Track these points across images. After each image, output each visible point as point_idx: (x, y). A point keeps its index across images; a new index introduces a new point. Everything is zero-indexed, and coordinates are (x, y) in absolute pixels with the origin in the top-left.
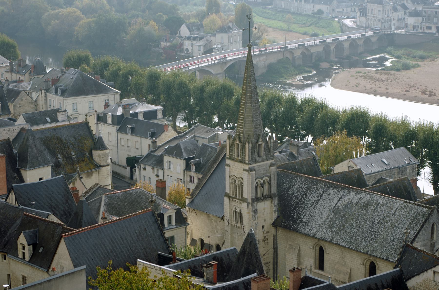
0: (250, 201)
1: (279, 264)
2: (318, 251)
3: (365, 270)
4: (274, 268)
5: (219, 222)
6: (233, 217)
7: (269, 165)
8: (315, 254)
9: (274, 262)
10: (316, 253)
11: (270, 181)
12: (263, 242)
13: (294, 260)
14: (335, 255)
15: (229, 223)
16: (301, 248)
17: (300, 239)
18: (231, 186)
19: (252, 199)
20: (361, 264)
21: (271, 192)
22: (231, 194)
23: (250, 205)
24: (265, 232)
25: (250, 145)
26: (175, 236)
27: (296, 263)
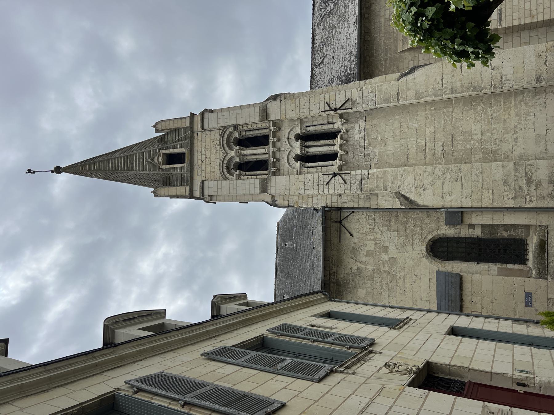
17: (383, 20)
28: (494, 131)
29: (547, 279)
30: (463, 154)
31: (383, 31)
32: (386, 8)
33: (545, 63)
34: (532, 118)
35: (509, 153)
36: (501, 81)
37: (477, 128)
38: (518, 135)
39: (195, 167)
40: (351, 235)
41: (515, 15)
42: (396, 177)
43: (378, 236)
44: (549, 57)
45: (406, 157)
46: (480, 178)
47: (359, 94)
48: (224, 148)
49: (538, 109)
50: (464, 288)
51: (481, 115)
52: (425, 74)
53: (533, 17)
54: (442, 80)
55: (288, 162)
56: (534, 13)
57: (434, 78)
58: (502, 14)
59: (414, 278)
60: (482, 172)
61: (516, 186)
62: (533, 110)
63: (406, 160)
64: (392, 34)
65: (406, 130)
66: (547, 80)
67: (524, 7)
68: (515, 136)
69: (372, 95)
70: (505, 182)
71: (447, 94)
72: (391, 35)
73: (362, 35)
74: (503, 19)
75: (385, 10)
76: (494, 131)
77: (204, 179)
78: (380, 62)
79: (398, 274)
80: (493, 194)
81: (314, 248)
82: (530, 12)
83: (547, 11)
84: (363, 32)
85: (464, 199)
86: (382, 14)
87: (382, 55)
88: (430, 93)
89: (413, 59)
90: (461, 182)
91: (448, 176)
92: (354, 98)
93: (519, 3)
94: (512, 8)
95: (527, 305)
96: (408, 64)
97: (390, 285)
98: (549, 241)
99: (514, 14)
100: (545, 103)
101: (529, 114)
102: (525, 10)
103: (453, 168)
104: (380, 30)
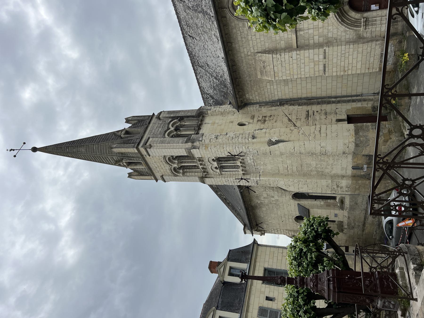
0: (189, 145)
1: (309, 95)
4: (318, 103)
5: (256, 193)
6: (231, 173)
9: (305, 104)
11: (178, 117)
12: (266, 123)
13: (283, 60)
15: (242, 179)
16: (260, 50)
17: (243, 55)
18: (188, 174)
19: (186, 142)
22: (199, 174)
23: (195, 144)
24: (251, 121)
26: (266, 266)
27: (287, 54)
28: (322, 165)
29: (343, 210)
30: (307, 171)
31: (244, 63)
32: (244, 47)
33: (348, 147)
34: (340, 161)
35: (329, 173)
36: (326, 152)
37: (314, 163)
38: (334, 167)
39: (153, 169)
40: (255, 192)
41: (334, 69)
42: (275, 181)
43: (268, 193)
44: (350, 145)
45: (278, 171)
46: (316, 184)
47: (247, 150)
48: (168, 164)
49: (343, 158)
50: (310, 212)
51: (316, 158)
52: (285, 145)
53: (345, 71)
54: (294, 148)
55: (212, 170)
56: (346, 69)
57: (290, 148)
58: (326, 68)
59: (287, 205)
60: (317, 183)
61: (332, 188)
62: (341, 158)
63: (278, 172)
64: (252, 65)
65: (277, 161)
66: (348, 154)
67: (340, 65)
68: (332, 167)
69: (255, 151)
70: (327, 186)
71: (297, 154)
72: (251, 66)
73: (230, 66)
74: (326, 71)
75: (244, 48)
76: (322, 165)
77: (161, 175)
78: (247, 82)
79: (280, 204)
80: (322, 189)
81: (234, 189)
82: (344, 68)
83: (354, 68)
84: (230, 64)
85: (308, 190)
86: (242, 51)
87: (247, 78)
88: (288, 153)
89: (269, 82)
90: (307, 185)
91: (301, 183)
92: (245, 151)
93: (337, 61)
94: (333, 64)
95: (335, 217)
96: (266, 85)
97: (277, 207)
98: (345, 201)
99: (334, 69)
100: (347, 156)
101: (339, 160)
102: (341, 66)
103: (303, 181)
104: (243, 62)
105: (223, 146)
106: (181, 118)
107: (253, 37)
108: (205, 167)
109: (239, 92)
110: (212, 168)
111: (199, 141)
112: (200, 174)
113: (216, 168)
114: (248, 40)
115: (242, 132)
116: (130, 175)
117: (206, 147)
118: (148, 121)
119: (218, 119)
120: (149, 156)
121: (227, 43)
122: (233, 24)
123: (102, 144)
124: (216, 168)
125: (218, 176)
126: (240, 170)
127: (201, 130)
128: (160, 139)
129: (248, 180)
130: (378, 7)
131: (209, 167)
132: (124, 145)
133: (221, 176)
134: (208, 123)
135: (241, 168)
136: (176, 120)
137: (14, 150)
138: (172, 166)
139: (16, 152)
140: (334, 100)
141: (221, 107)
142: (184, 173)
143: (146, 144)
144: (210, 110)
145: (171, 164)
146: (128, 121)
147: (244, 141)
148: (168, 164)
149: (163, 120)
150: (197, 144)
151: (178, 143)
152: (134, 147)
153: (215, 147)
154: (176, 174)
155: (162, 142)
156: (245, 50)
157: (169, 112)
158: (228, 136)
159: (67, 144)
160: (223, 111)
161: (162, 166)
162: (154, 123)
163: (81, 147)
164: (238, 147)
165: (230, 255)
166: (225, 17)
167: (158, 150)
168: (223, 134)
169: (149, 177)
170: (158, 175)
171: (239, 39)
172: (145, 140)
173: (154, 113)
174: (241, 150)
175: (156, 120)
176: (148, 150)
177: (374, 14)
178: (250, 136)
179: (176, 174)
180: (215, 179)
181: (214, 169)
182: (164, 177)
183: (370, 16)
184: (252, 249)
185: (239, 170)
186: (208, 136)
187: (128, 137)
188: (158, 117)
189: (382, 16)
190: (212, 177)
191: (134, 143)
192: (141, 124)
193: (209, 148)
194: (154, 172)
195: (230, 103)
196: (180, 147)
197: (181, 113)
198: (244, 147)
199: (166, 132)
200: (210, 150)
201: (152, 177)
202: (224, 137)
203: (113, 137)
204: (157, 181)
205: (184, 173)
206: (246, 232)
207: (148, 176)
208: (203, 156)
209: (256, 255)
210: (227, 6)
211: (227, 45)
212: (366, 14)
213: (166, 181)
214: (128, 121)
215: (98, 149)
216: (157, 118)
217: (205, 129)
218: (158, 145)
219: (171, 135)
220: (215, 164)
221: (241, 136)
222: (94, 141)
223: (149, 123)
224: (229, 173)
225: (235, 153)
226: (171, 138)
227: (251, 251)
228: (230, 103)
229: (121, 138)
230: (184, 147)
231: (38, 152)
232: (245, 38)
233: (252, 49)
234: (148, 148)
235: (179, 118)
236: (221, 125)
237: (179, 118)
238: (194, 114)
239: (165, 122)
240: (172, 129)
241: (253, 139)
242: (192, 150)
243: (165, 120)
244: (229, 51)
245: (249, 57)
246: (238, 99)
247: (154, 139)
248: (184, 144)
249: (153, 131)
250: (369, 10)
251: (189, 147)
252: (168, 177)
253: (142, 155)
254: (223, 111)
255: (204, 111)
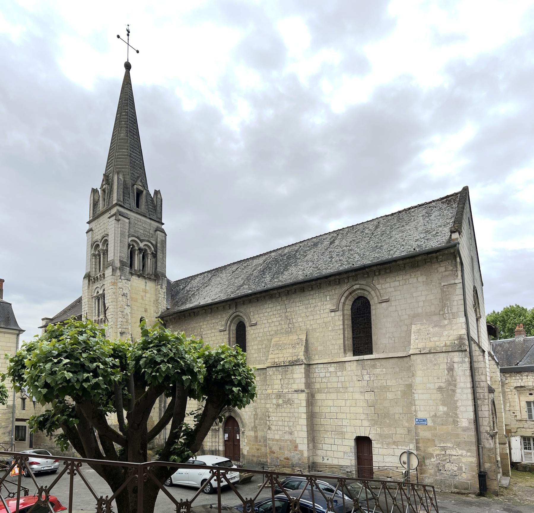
0: (118, 265)
2: (235, 332)
3: (343, 320)
6: (94, 309)
7: (155, 229)
8: (229, 338)
10: (231, 336)
11: (156, 251)
14: (270, 321)
17: (201, 324)
18: (94, 260)
19: (121, 261)
20: (332, 311)
21: (156, 268)
22: (94, 273)
23: (118, 271)
25: (121, 177)
39: (98, 220)
48: (102, 239)
55: (96, 288)
84: (195, 310)
104: (196, 323)
105: (114, 302)
106: (155, 256)
107: (213, 334)
108: (99, 280)
109: (174, 318)
110: (98, 288)
111: (121, 276)
112: (93, 274)
113: (98, 292)
114: (212, 329)
115: (130, 321)
116: (94, 191)
117: (114, 284)
118: (154, 217)
119: (150, 296)
120: (109, 218)
121: (211, 309)
122: (224, 315)
123: (127, 160)
124: (98, 292)
125: (90, 294)
126: (96, 318)
127: (137, 278)
128: (127, 231)
129: (106, 321)
130: (226, 439)
131: (98, 285)
132: (121, 189)
133: (90, 297)
134: (146, 286)
135: (97, 319)
136: (153, 249)
137: (128, 35)
138: (101, 242)
139: (125, 38)
140: (163, 405)
141: (164, 300)
142: (94, 255)
143: (120, 215)
144: (161, 288)
145: (102, 241)
146: (157, 193)
147: (119, 323)
148: (102, 239)
149: (155, 234)
150: (118, 273)
151: (120, 252)
152: (118, 200)
153: (114, 293)
154: (94, 247)
155: (122, 234)
156: (205, 326)
157: (164, 242)
158: (126, 307)
159: (131, 113)
160: (159, 301)
161: (100, 232)
162: (152, 225)
163: (126, 132)
164: (112, 318)
165: (4, 304)
166: (230, 308)
167: (113, 229)
168: (129, 302)
169: (92, 215)
170: (93, 225)
171: (213, 321)
172: (127, 214)
173: (163, 224)
174: (110, 320)
175: (155, 227)
176: (114, 218)
177: (221, 436)
178: (123, 330)
179: (94, 247)
180: (87, 291)
181: (96, 291)
182: (91, 232)
183: (219, 434)
184: (12, 328)
185: (96, 317)
186: (127, 286)
187: (134, 193)
188: (158, 229)
189: (218, 442)
190: (89, 287)
191: (124, 201)
192: (150, 209)
193: (113, 287)
194: (96, 221)
195: (168, 309)
196: (116, 254)
197: (162, 255)
198: (112, 323)
199: (138, 238)
200: (110, 287)
201: (91, 218)
202: (125, 303)
203: (136, 174)
204: (89, 223)
205: (94, 255)
206: (44, 321)
207: (93, 214)
208: (106, 279)
209: (5, 333)
210: (237, 311)
211: (209, 309)
212: (221, 430)
213: (88, 234)
214: (157, 193)
215: (122, 155)
216: (158, 227)
217: (137, 283)
218: (119, 229)
219: (134, 244)
220: (101, 292)
221: (125, 320)
222: (132, 150)
223: (151, 219)
224: (94, 306)
225: (108, 313)
226: (127, 244)
227: (9, 327)
228: (168, 309)
229: (133, 185)
230: (116, 258)
231: (124, 70)
232: (214, 326)
233: (205, 332)
234: (116, 217)
235: (154, 253)
236: (142, 299)
237: (154, 253)
238: (159, 269)
239: (152, 237)
240: (142, 245)
241: (120, 333)
242: (111, 267)
243: (155, 237)
244: (205, 310)
245: (199, 330)
246: (168, 318)
247: (127, 225)
248: (118, 258)
249: (140, 224)
250: (225, 432)
251: (116, 264)
252: (90, 236)
253: (110, 209)
254: (159, 301)
255: (160, 281)
